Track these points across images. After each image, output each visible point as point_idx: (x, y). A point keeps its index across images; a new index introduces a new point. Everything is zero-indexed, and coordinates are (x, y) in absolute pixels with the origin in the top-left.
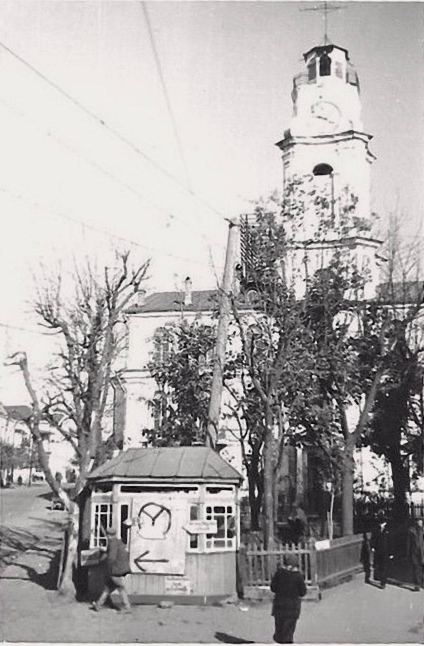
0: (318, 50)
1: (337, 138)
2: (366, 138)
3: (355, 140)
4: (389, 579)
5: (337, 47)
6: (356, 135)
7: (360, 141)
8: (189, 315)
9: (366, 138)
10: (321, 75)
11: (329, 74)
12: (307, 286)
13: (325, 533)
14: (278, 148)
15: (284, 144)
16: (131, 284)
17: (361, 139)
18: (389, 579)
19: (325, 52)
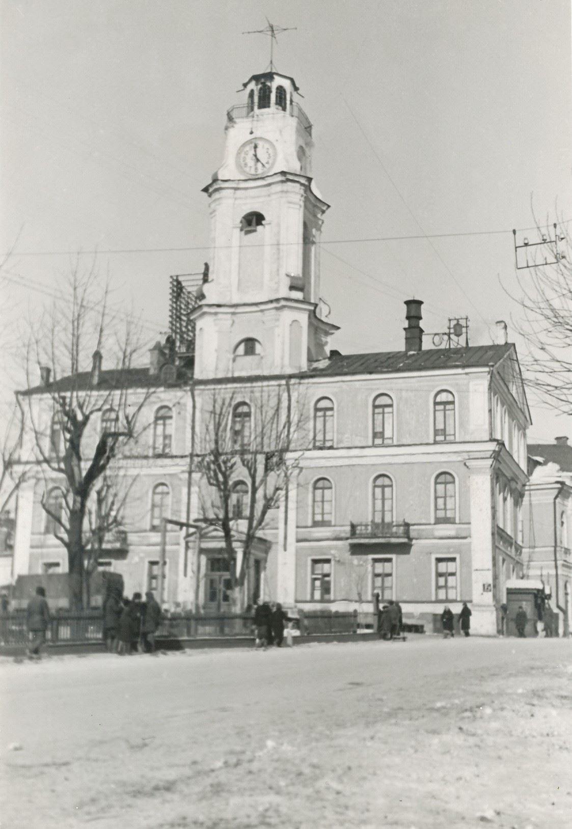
0: (256, 78)
1: (269, 180)
2: (303, 181)
3: (289, 184)
4: (101, 560)
5: (277, 74)
6: (291, 177)
7: (298, 185)
8: (241, 634)
9: (303, 181)
10: (260, 107)
11: (269, 107)
12: (366, 525)
13: (181, 822)
14: (205, 195)
15: (211, 190)
16: (99, 410)
17: (298, 182)
18: (101, 560)
19: (263, 80)
